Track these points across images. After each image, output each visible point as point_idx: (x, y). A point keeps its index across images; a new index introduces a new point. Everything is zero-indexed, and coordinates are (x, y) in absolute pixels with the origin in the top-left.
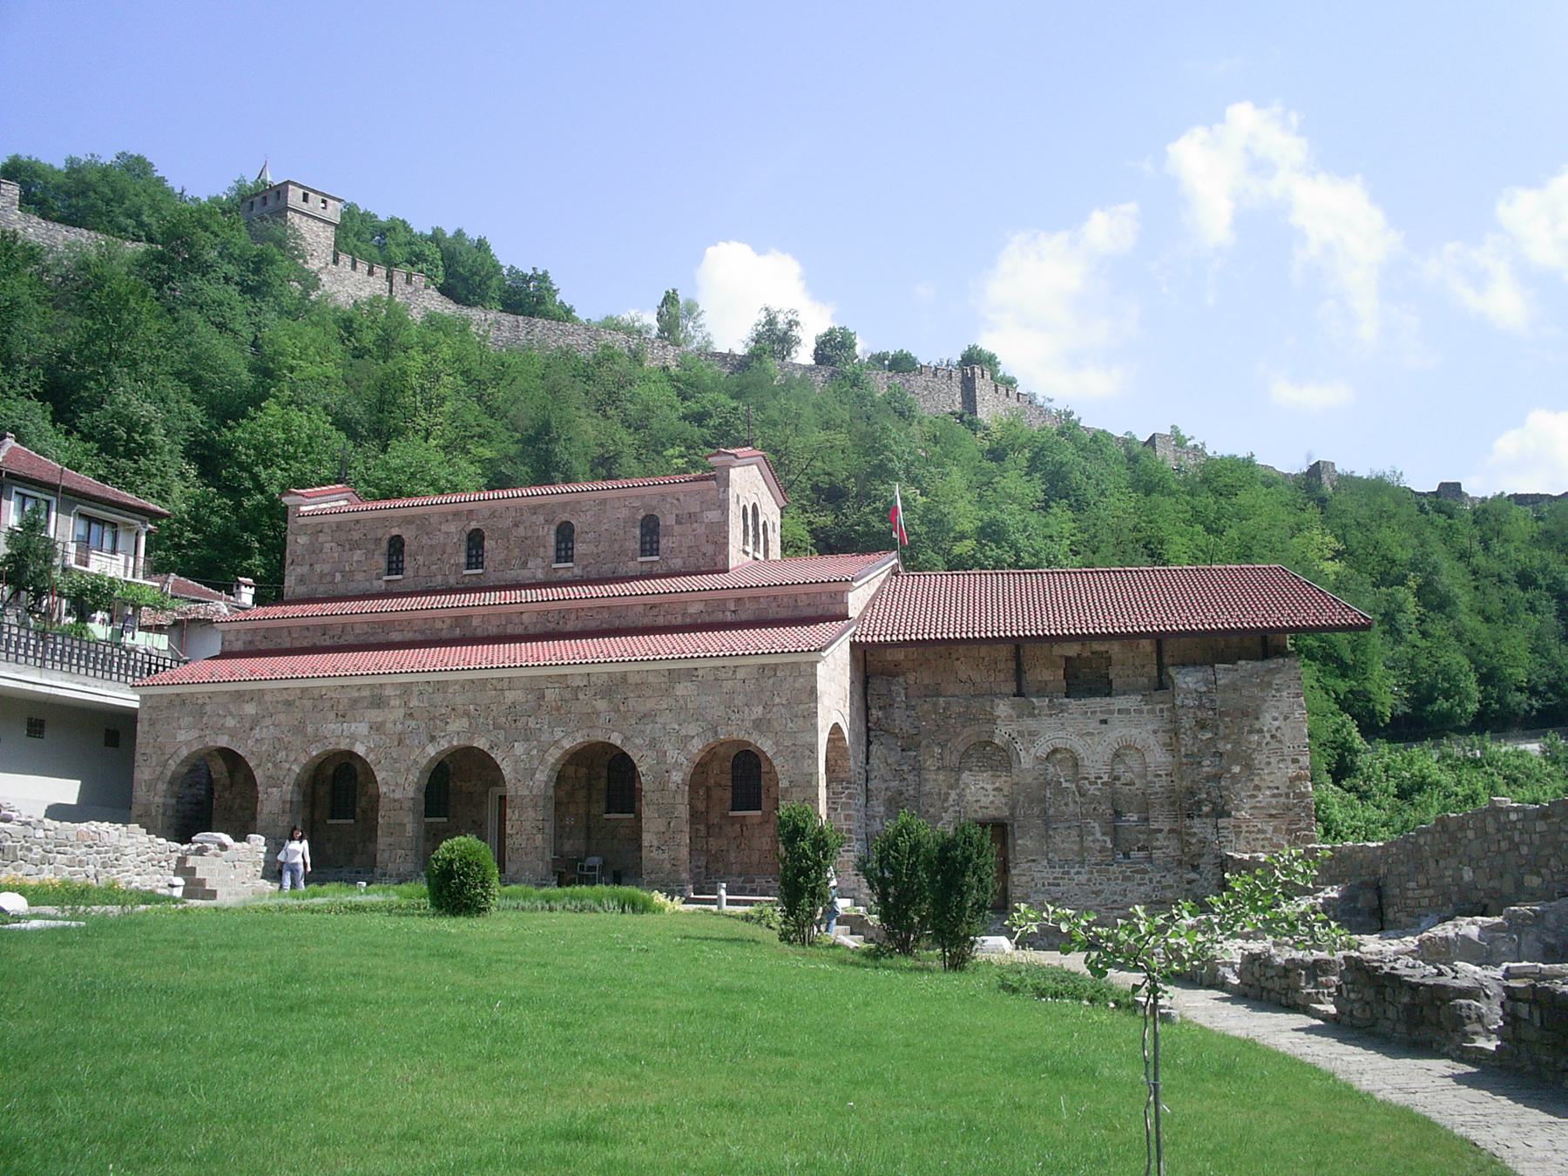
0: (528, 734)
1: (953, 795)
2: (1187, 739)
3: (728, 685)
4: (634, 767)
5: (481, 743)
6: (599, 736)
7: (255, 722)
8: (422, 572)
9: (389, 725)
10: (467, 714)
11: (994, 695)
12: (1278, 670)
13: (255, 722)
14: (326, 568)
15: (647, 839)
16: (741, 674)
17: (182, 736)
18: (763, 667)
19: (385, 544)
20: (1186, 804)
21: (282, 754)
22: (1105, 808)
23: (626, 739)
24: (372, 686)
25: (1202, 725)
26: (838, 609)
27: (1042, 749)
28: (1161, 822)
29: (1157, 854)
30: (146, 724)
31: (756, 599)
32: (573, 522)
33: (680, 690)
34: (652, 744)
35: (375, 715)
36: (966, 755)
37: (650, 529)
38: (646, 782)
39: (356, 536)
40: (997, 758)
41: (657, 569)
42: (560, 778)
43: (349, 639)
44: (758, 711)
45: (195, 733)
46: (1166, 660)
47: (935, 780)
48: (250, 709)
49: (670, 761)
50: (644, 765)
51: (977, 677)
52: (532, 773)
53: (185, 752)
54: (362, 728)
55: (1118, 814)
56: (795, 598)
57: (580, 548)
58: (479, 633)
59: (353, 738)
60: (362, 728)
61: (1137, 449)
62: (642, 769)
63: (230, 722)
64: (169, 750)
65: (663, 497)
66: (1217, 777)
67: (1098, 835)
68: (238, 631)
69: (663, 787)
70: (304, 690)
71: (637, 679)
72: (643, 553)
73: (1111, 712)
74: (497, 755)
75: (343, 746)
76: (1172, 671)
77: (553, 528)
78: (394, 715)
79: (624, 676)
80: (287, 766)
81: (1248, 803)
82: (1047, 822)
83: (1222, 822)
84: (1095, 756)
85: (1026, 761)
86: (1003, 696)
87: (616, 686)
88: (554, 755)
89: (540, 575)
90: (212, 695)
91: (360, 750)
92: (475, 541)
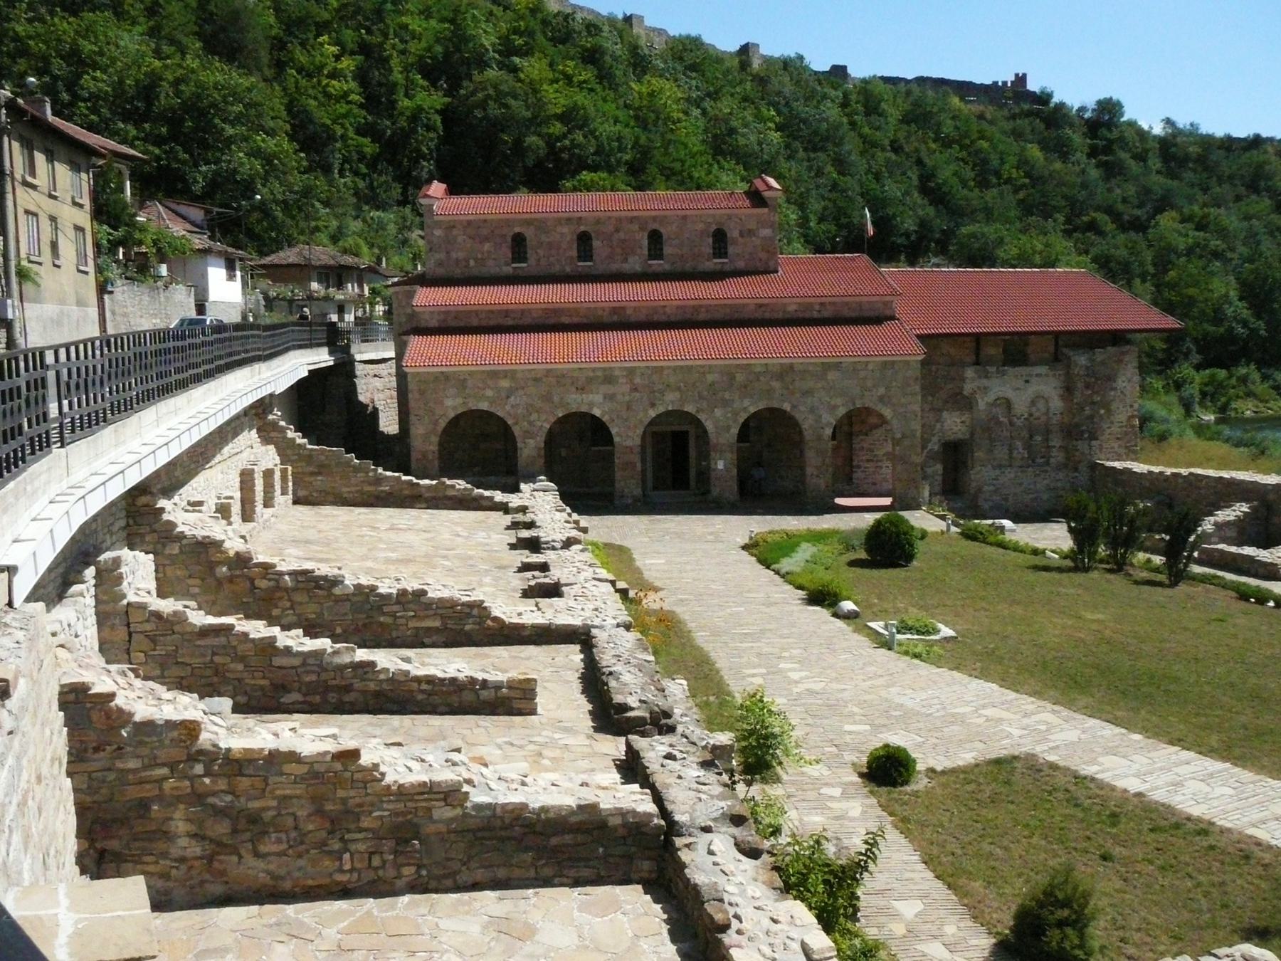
0: (725, 403)
1: (938, 426)
2: (1078, 394)
3: (862, 374)
5: (689, 408)
8: (543, 262)
9: (619, 397)
10: (679, 389)
11: (963, 365)
12: (1127, 352)
14: (461, 255)
15: (809, 470)
18: (885, 363)
19: (509, 239)
21: (534, 416)
22: (1025, 434)
23: (794, 407)
24: (604, 369)
25: (1087, 386)
26: (888, 313)
27: (991, 397)
28: (1056, 442)
29: (1052, 460)
30: (417, 396)
31: (834, 304)
32: (662, 230)
33: (832, 376)
34: (812, 410)
35: (609, 389)
37: (720, 240)
38: (808, 435)
39: (485, 232)
41: (727, 268)
43: (527, 321)
44: (882, 390)
45: (459, 401)
46: (1061, 343)
48: (505, 384)
49: (824, 421)
50: (807, 424)
52: (728, 428)
53: (452, 414)
54: (598, 398)
55: (1031, 437)
56: (860, 304)
57: (667, 250)
58: (633, 319)
59: (591, 404)
60: (598, 398)
62: (805, 426)
63: (489, 393)
64: (439, 412)
65: (730, 217)
66: (1091, 417)
67: (1020, 450)
68: (432, 313)
69: (819, 438)
70: (549, 371)
71: (801, 367)
73: (1031, 375)
74: (702, 417)
75: (584, 409)
76: (1065, 350)
77: (646, 235)
78: (622, 388)
79: (791, 366)
80: (539, 424)
81: (1108, 431)
83: (1094, 443)
85: (982, 405)
87: (786, 373)
89: (638, 268)
90: (471, 374)
91: (597, 412)
92: (584, 240)
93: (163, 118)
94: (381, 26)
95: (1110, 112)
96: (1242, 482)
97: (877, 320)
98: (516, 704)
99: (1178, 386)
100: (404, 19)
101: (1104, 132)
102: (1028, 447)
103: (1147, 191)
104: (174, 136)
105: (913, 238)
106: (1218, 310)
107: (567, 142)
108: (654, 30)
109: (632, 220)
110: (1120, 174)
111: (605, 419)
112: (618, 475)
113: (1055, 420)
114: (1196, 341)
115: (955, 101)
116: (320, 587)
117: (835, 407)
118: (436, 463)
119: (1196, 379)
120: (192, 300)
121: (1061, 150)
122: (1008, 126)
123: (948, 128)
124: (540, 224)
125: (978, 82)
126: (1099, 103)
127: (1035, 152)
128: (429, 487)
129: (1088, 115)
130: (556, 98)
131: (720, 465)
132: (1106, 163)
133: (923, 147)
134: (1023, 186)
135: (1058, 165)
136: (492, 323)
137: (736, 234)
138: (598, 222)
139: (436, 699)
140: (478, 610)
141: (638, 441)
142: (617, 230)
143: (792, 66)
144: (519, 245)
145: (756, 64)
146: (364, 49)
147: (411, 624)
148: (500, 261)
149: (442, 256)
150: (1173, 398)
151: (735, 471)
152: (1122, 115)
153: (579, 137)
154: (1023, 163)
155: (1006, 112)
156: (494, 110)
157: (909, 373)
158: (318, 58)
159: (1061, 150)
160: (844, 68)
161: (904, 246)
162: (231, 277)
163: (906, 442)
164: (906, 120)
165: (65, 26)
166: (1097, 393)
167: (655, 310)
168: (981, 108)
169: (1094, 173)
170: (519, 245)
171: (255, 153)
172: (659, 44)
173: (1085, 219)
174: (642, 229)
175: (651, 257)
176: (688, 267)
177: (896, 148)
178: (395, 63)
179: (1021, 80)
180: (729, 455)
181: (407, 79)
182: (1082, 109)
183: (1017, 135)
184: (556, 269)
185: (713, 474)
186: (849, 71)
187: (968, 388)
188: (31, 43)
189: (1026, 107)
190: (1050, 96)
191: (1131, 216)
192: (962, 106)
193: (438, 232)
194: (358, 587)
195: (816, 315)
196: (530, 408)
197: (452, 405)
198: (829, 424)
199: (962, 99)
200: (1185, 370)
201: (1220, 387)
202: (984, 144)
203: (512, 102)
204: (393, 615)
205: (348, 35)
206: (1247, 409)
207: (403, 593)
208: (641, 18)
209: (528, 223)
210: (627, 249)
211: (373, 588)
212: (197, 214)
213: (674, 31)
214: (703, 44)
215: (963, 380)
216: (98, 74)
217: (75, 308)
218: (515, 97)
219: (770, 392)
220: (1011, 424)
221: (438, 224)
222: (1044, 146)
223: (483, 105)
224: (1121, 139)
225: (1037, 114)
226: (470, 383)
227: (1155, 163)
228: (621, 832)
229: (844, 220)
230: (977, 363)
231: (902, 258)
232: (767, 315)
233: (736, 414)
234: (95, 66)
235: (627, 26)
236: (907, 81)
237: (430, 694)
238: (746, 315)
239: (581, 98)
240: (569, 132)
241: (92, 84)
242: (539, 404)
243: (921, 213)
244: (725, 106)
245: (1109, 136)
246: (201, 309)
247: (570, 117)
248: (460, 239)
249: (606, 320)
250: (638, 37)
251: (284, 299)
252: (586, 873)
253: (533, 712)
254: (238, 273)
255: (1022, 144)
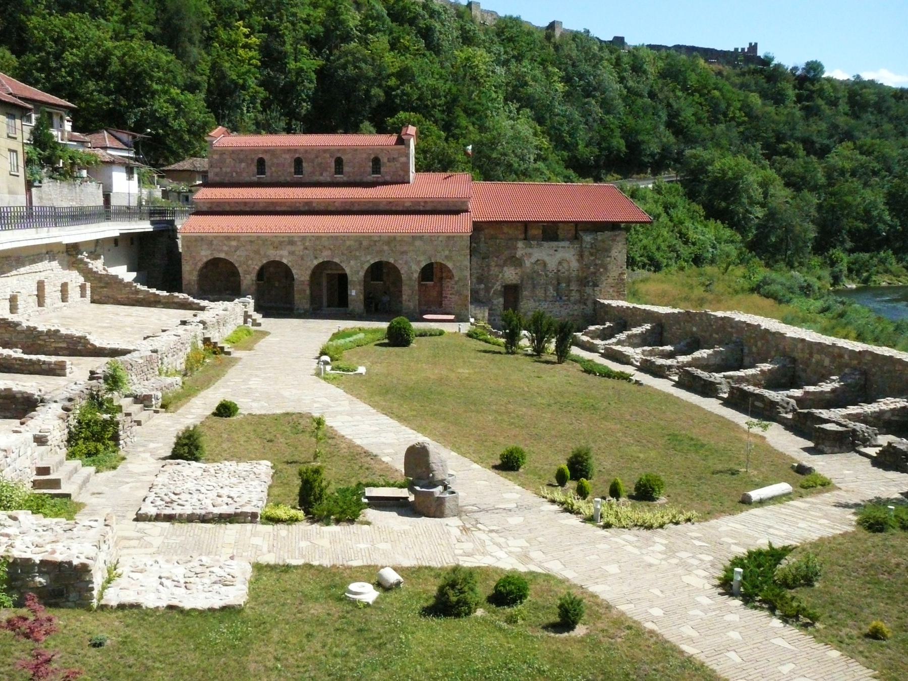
0: (356, 258)
1: (501, 276)
3: (435, 243)
4: (399, 271)
5: (336, 260)
6: (384, 259)
7: (237, 248)
8: (275, 174)
11: (517, 239)
12: (618, 235)
13: (237, 248)
14: (228, 170)
16: (440, 239)
17: (203, 253)
20: (583, 282)
21: (250, 262)
22: (555, 282)
23: (395, 261)
25: (592, 254)
26: (465, 208)
27: (533, 260)
28: (574, 287)
29: (572, 298)
33: (418, 243)
35: (290, 248)
36: (505, 261)
38: (404, 277)
39: (241, 156)
40: (517, 262)
41: (380, 180)
42: (366, 276)
44: (447, 253)
45: (209, 252)
46: (579, 228)
47: (494, 270)
48: (234, 243)
51: (510, 232)
52: (358, 272)
53: (205, 260)
57: (346, 169)
58: (316, 209)
59: (282, 256)
60: (285, 253)
61: (462, 9)
62: (402, 272)
63: (225, 248)
64: (198, 259)
66: (595, 273)
67: (551, 291)
69: (410, 279)
70: (258, 237)
72: (374, 173)
76: (581, 233)
77: (333, 160)
78: (298, 248)
82: (534, 287)
84: (552, 264)
86: (521, 240)
87: (391, 241)
88: (366, 266)
89: (329, 179)
91: (285, 261)
92: (298, 163)
93: (110, 79)
94: (278, 14)
95: (815, 70)
96: (653, 313)
97: (456, 212)
98: (58, 372)
99: (833, 264)
100: (294, 10)
101: (808, 84)
102: (557, 289)
103: (835, 127)
104: (118, 91)
105: (656, 158)
106: (867, 212)
107: (399, 91)
108: (488, 12)
109: (325, 151)
110: (816, 115)
111: (289, 265)
112: (297, 296)
113: (574, 274)
114: (849, 232)
115: (702, 62)
116: (10, 326)
117: (419, 262)
118: (196, 287)
119: (844, 260)
120: (101, 192)
121: (778, 99)
122: (738, 80)
123: (693, 79)
124: (271, 151)
125: (719, 49)
126: (808, 64)
127: (755, 99)
128: (165, 297)
129: (798, 73)
130: (392, 61)
131: (354, 293)
132: (807, 106)
133: (671, 95)
134: (744, 122)
135: (771, 109)
136: (237, 209)
137: (385, 160)
138: (306, 151)
139: (24, 368)
140: (83, 340)
141: (308, 278)
142: (317, 157)
143: (580, 39)
144: (261, 164)
145: (557, 33)
146: (267, 29)
147: (53, 345)
148: (250, 173)
149: (218, 170)
150: (826, 273)
151: (362, 297)
152: (823, 73)
153: (407, 88)
154: (746, 108)
155: (738, 71)
156: (351, 71)
157: (464, 243)
158: (234, 36)
159: (778, 99)
160: (622, 39)
161: (651, 163)
162: (130, 178)
163: (461, 284)
164: (663, 75)
165: (57, 21)
166: (599, 259)
167: (329, 203)
168: (721, 67)
169: (798, 114)
170: (261, 164)
171: (173, 101)
172: (490, 21)
173: (784, 146)
174: (331, 157)
175: (336, 173)
176: (358, 179)
177: (652, 95)
178: (289, 39)
179: (753, 48)
180: (358, 287)
181: (295, 49)
182: (795, 69)
183: (743, 86)
184: (282, 179)
185: (349, 298)
186: (626, 40)
187: (519, 254)
188: (36, 32)
189: (752, 66)
190: (772, 59)
191: (822, 145)
192: (706, 65)
193: (215, 157)
194: (28, 327)
195: (421, 208)
196: (248, 258)
197: (205, 255)
198: (416, 271)
199: (706, 61)
200: (837, 253)
201: (865, 266)
202: (716, 93)
203: (363, 65)
204: (44, 340)
205: (257, 19)
206: (884, 281)
207: (49, 331)
208: (478, 4)
209: (266, 151)
210: (323, 168)
211: (35, 328)
212: (125, 137)
213: (502, 14)
214: (522, 22)
215: (516, 248)
216: (74, 50)
217: (7, 195)
218: (366, 62)
219: (381, 252)
220: (547, 276)
221: (215, 152)
222: (764, 95)
223: (344, 67)
224: (821, 90)
225: (761, 72)
226: (215, 242)
227: (843, 107)
228: (21, 400)
229: (604, 145)
230: (525, 239)
231: (649, 171)
232: (394, 208)
233: (362, 264)
234: (72, 46)
235: (468, 10)
236: (666, 48)
237: (21, 365)
238: (381, 207)
239: (409, 61)
240: (402, 84)
241: (70, 57)
242: (252, 255)
243: (665, 140)
244: (526, 66)
245: (811, 87)
246: (107, 198)
247: (404, 75)
248: (228, 161)
249: (302, 209)
250: (476, 17)
251: (175, 191)
252: (8, 414)
253: (64, 375)
254: (136, 176)
255: (747, 92)
